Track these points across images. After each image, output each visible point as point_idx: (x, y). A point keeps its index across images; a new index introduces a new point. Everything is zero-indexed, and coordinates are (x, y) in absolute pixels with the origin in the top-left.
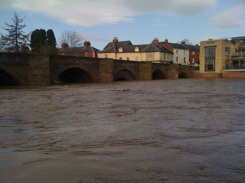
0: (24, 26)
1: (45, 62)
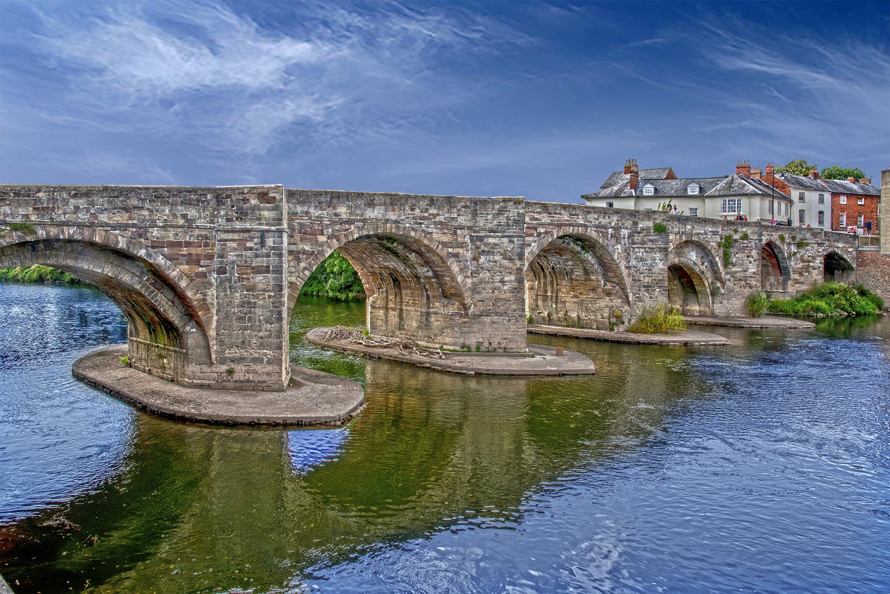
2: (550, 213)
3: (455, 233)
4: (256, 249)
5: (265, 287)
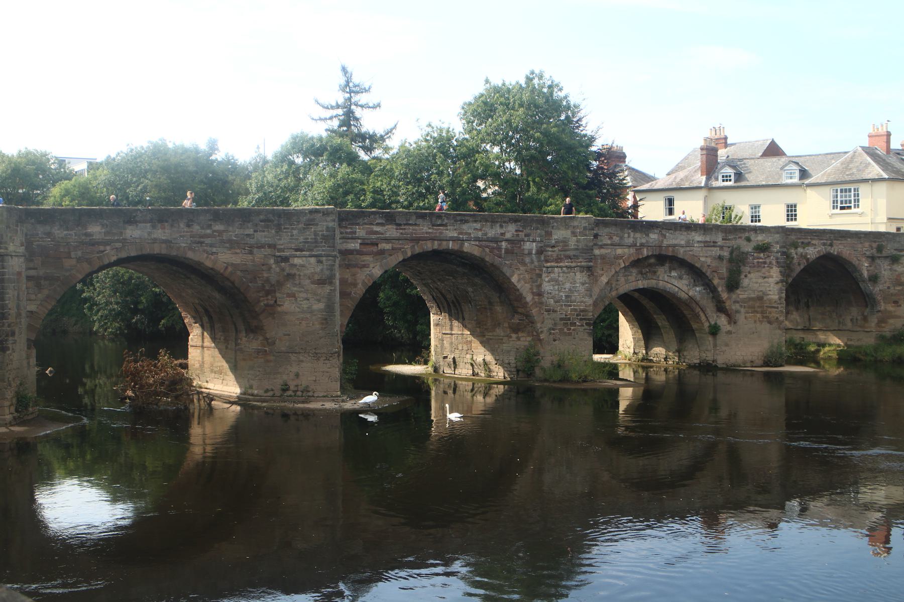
3: (251, 253)
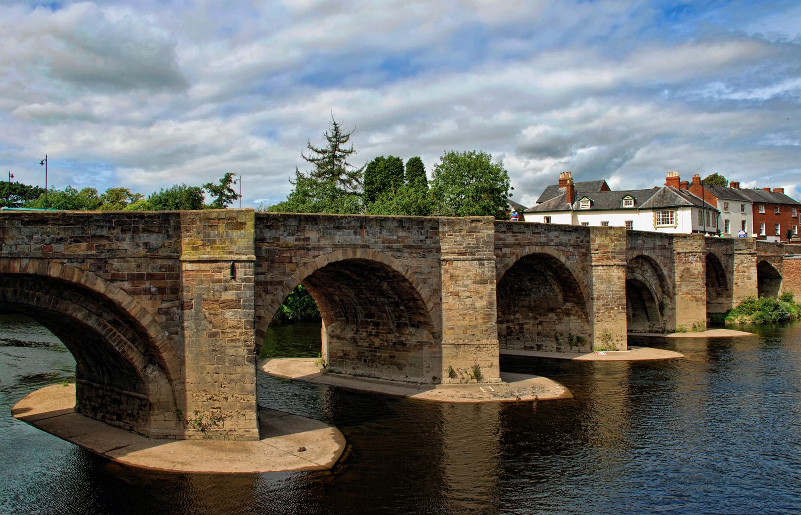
0: (351, 152)
1: (484, 241)
2: (514, 233)
4: (226, 281)
5: (235, 323)
